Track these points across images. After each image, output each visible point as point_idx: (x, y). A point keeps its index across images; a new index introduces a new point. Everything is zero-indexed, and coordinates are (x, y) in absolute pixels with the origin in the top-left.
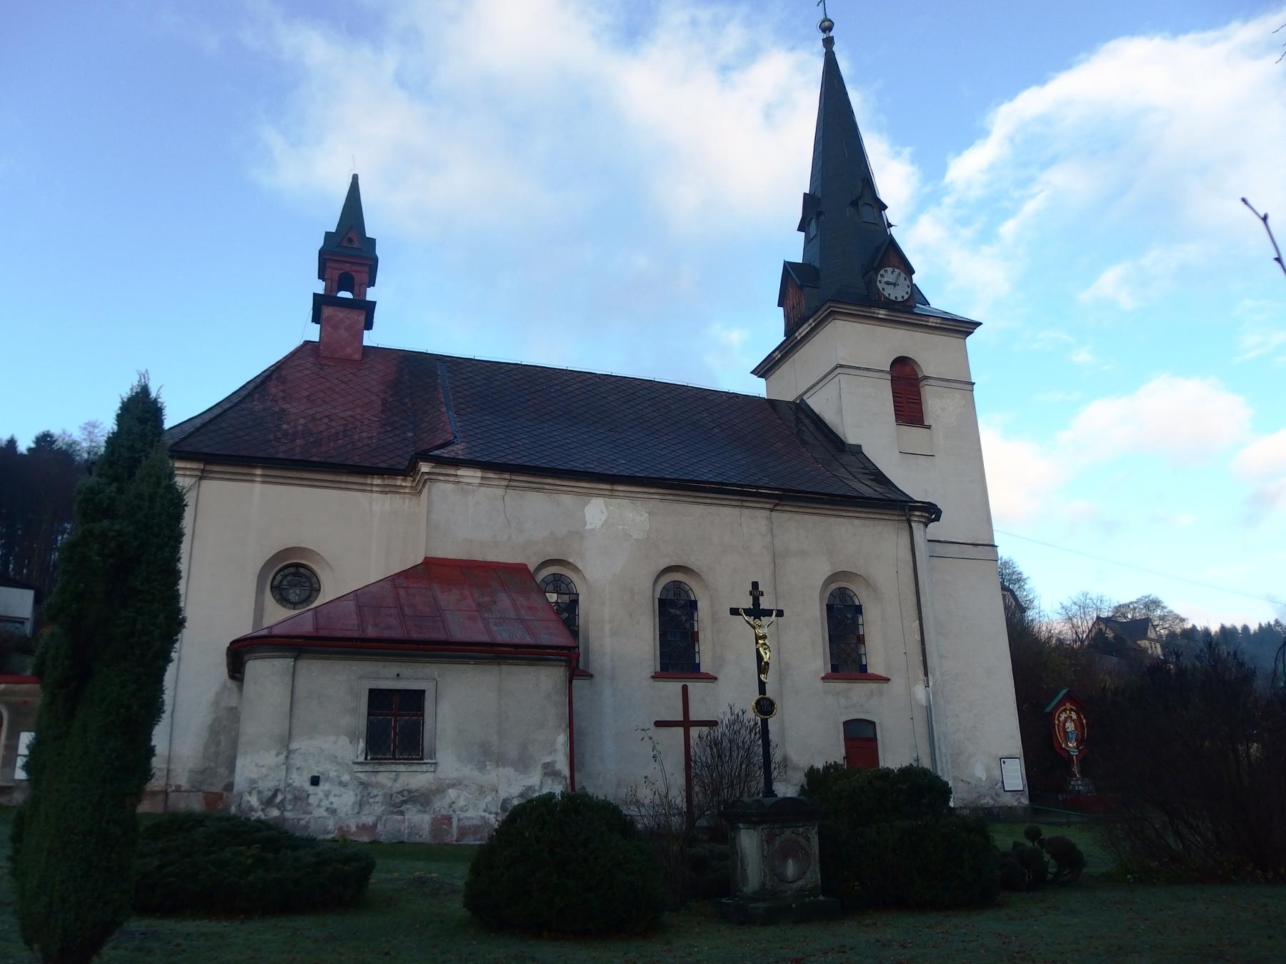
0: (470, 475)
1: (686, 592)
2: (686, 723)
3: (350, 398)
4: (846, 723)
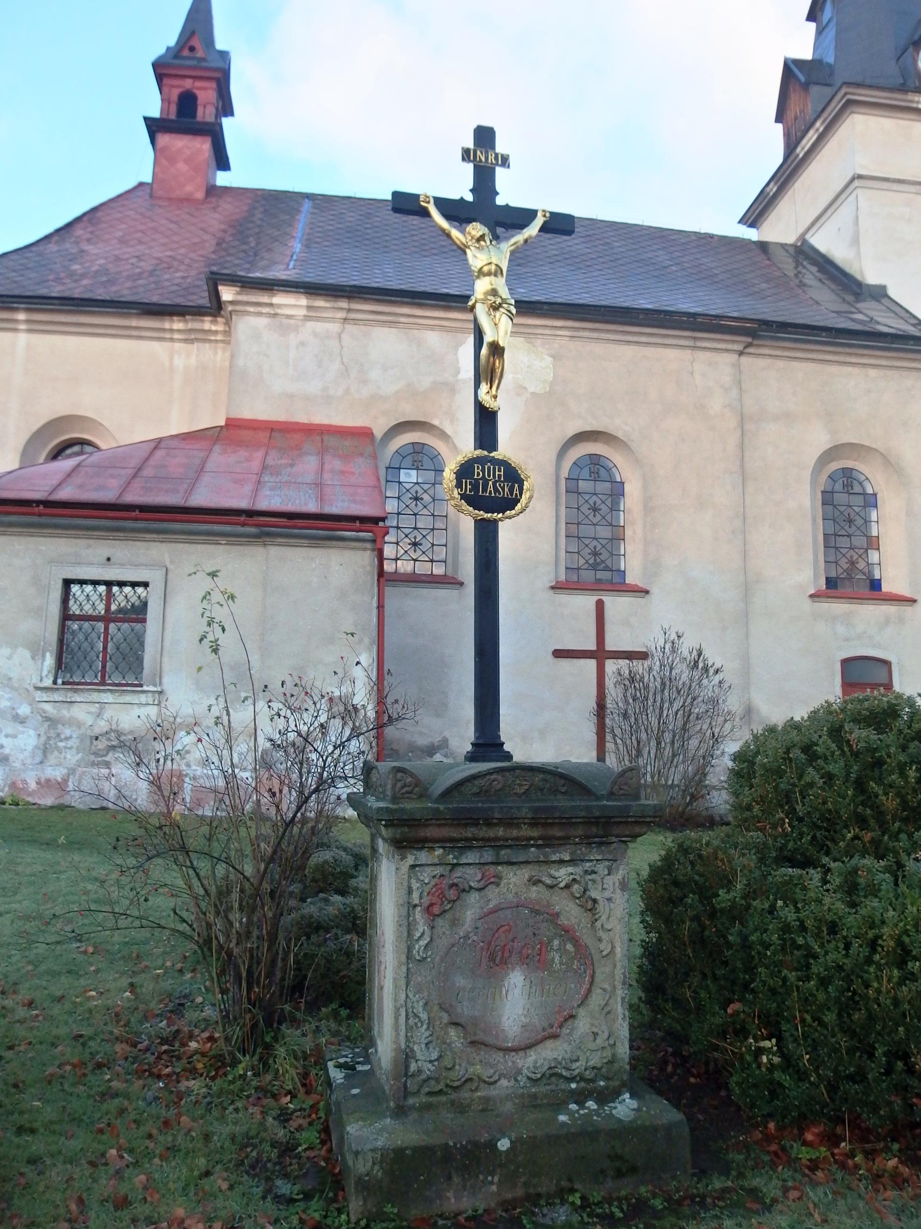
0: (292, 304)
1: (608, 470)
2: (600, 654)
3: (175, 238)
4: (845, 662)
